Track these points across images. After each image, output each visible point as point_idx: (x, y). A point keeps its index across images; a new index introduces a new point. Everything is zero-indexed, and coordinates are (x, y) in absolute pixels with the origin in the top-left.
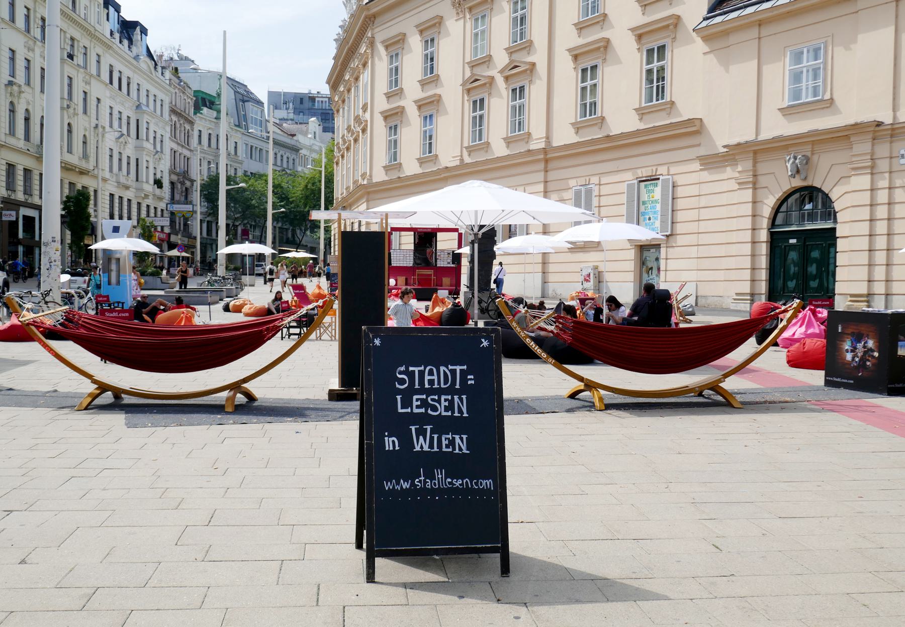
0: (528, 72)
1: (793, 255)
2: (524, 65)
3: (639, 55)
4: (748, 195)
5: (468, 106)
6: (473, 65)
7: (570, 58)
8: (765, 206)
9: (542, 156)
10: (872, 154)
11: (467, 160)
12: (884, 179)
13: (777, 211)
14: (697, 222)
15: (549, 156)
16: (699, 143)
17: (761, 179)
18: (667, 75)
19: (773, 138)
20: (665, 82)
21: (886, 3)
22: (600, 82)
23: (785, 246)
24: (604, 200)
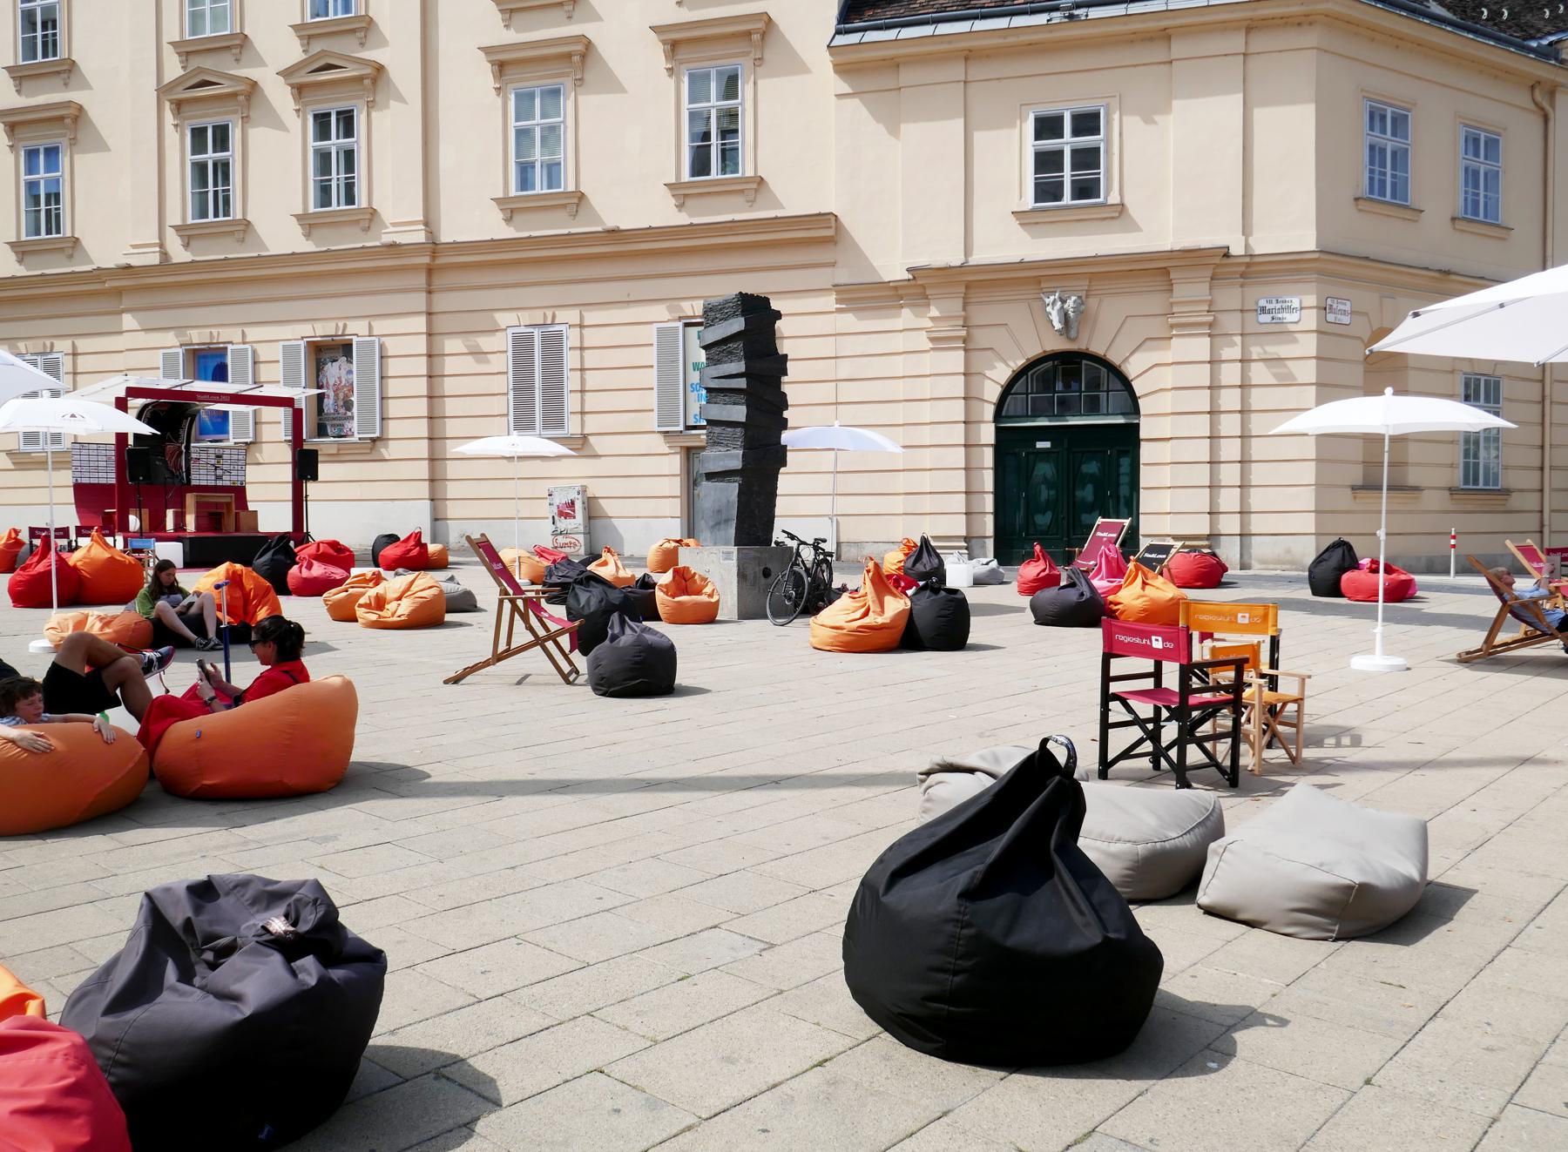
0: (576, 59)
1: (1044, 469)
2: (356, 66)
3: (11, 157)
4: (955, 361)
5: (177, 144)
6: (187, 51)
7: (486, 70)
8: (987, 383)
9: (426, 260)
10: (1211, 303)
11: (179, 254)
12: (1233, 344)
13: (1007, 390)
14: (835, 406)
15: (440, 261)
16: (833, 261)
17: (976, 333)
18: (746, 124)
19: (1021, 262)
20: (61, 206)
21: (1226, 55)
22: (67, 177)
23: (1027, 454)
24: (591, 359)
